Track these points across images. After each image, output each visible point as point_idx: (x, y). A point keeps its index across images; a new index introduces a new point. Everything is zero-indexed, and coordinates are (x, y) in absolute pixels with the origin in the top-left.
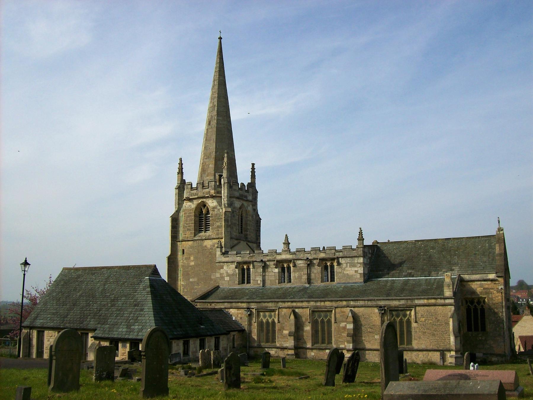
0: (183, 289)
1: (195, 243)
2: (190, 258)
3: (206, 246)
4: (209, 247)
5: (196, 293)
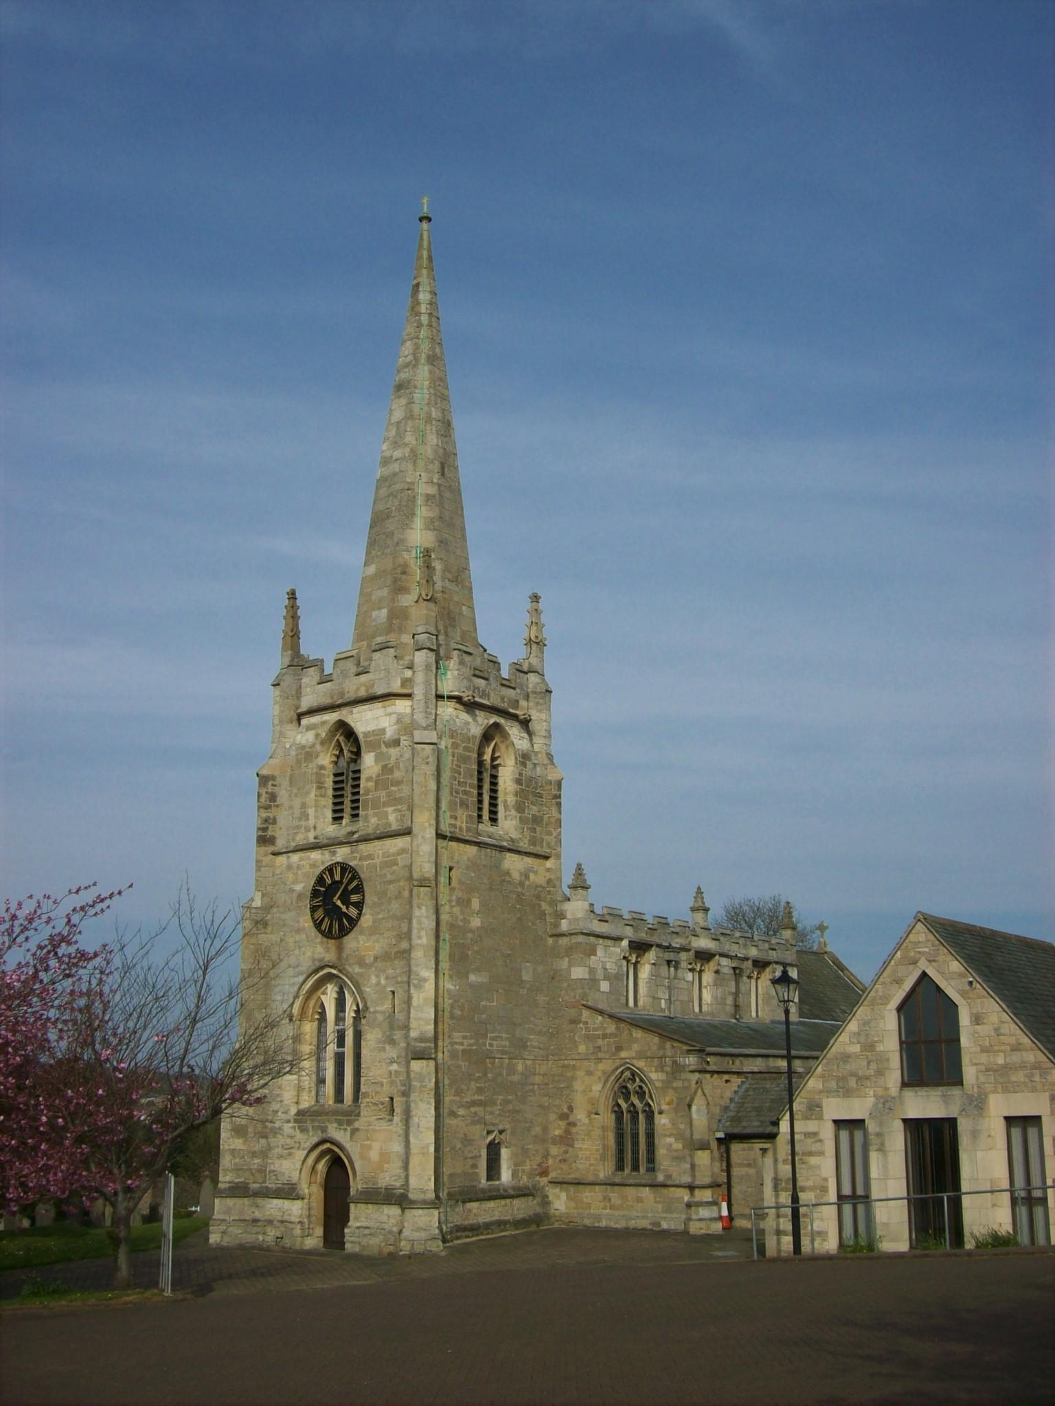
0: (452, 1007)
1: (483, 853)
2: (469, 901)
3: (508, 873)
4: (516, 876)
5: (486, 1024)
